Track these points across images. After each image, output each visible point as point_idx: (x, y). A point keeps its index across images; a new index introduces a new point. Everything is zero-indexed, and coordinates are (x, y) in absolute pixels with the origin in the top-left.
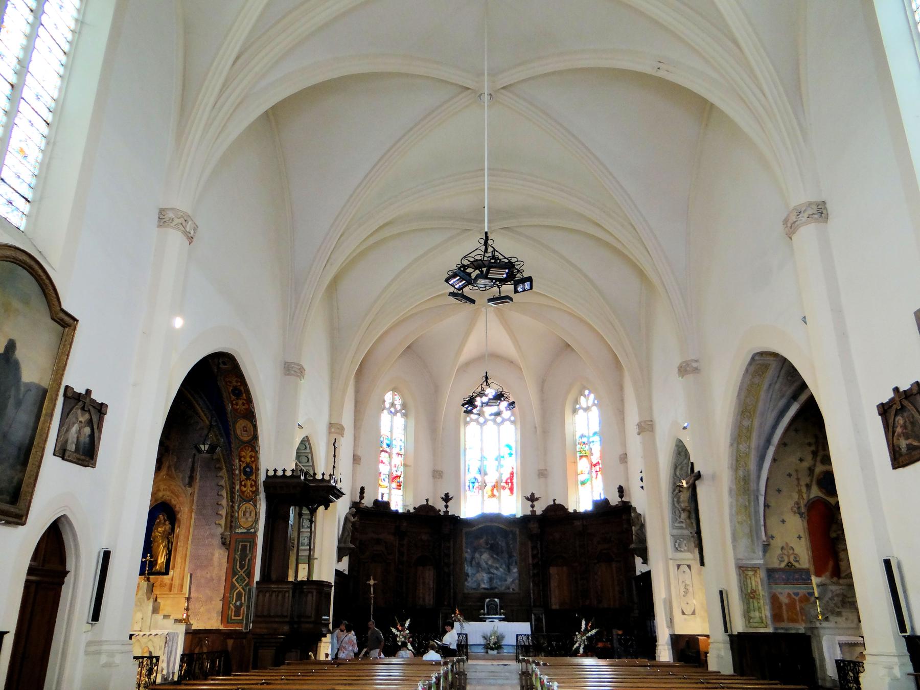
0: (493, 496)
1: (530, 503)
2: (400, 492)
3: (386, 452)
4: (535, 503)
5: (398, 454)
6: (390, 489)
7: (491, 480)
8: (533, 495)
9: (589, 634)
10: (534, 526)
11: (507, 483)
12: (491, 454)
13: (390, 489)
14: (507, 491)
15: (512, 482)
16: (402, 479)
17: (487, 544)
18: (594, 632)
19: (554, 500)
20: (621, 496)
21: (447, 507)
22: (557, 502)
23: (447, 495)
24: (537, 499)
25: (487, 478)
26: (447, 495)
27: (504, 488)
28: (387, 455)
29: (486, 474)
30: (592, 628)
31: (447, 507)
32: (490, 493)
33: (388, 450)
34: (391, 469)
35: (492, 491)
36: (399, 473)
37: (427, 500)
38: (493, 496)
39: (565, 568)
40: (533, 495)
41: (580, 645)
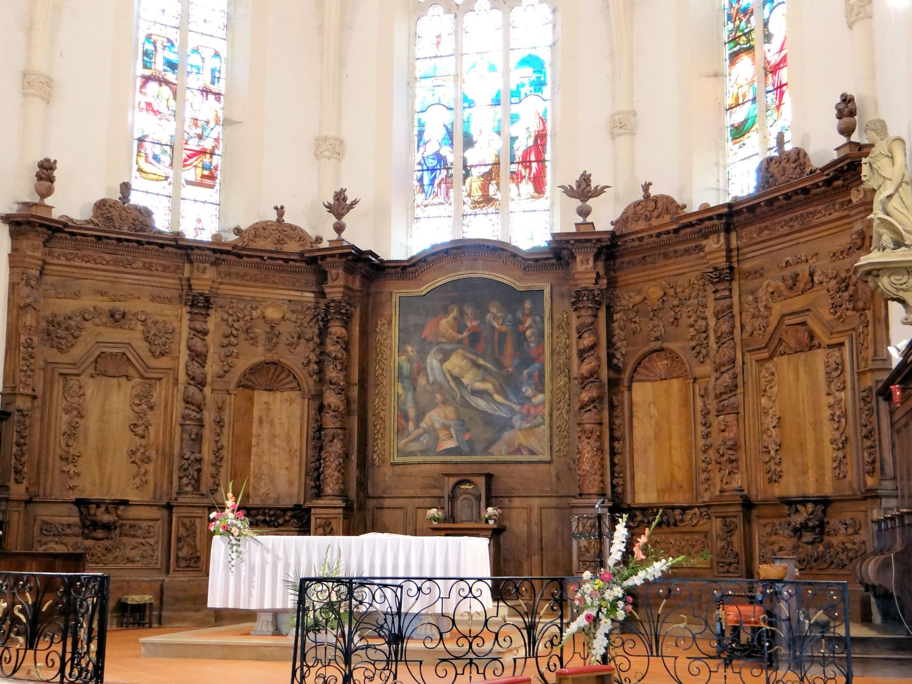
0: (487, 200)
1: (577, 203)
2: (212, 195)
3: (162, 81)
4: (591, 202)
5: (206, 91)
6: (177, 186)
7: (482, 154)
8: (586, 179)
9: (637, 580)
10: (585, 269)
11: (526, 163)
12: (482, 88)
13: (177, 186)
14: (527, 187)
15: (541, 161)
16: (216, 160)
17: (460, 328)
18: (657, 568)
19: (646, 187)
20: (847, 131)
21: (339, 229)
22: (653, 192)
23: (340, 196)
24: (599, 192)
25: (472, 156)
26: (340, 196)
27: (516, 177)
28: (166, 90)
29: (469, 142)
30: (651, 555)
31: (339, 229)
32: (477, 194)
33: (170, 76)
34: (181, 130)
35: (484, 188)
36: (208, 144)
37: (280, 211)
38: (487, 200)
39: (676, 384)
40: (586, 179)
41: (594, 621)
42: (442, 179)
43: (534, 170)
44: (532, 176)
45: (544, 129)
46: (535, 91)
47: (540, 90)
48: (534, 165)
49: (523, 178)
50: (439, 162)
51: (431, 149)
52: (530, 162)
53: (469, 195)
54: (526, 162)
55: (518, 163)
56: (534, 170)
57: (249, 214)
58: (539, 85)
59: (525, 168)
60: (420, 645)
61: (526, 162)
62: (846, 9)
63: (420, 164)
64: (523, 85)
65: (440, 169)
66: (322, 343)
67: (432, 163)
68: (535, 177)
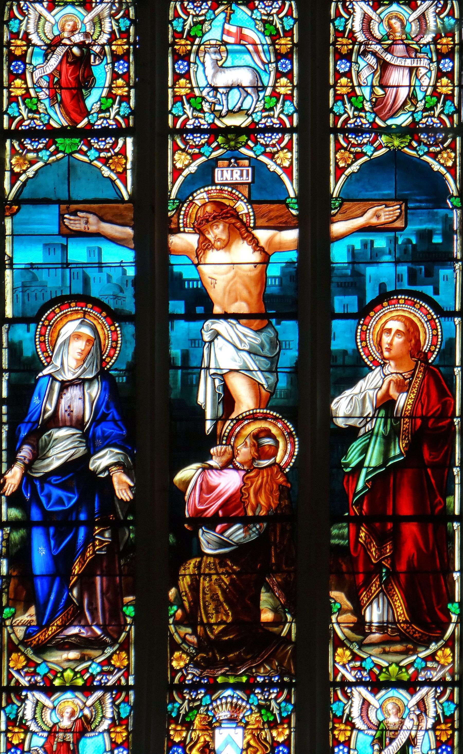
42: (97, 558)
43: (409, 548)
44: (402, 567)
45: (446, 411)
46: (413, 279)
47: (431, 277)
48: (410, 530)
49: (373, 571)
50: (84, 501)
51: (62, 448)
52: (399, 520)
53: (190, 619)
54: (384, 519)
55: (357, 521)
56: (409, 548)
57: (119, 306)
58: (426, 259)
59: (380, 538)
60: (383, 675)
61: (384, 519)
62: (231, 117)
63: (15, 500)
64: (374, 258)
65: (90, 525)
66: (233, 452)
67: (60, 499)
68: (412, 572)
